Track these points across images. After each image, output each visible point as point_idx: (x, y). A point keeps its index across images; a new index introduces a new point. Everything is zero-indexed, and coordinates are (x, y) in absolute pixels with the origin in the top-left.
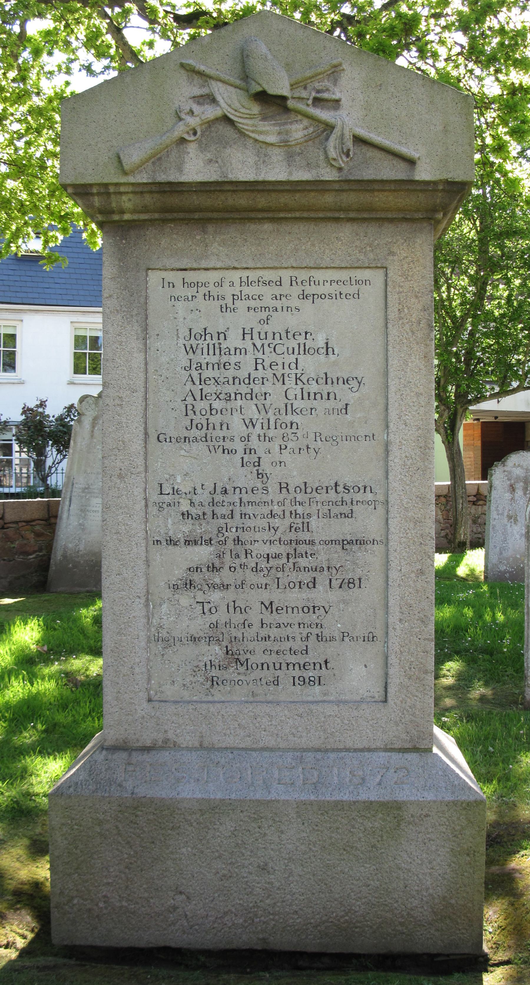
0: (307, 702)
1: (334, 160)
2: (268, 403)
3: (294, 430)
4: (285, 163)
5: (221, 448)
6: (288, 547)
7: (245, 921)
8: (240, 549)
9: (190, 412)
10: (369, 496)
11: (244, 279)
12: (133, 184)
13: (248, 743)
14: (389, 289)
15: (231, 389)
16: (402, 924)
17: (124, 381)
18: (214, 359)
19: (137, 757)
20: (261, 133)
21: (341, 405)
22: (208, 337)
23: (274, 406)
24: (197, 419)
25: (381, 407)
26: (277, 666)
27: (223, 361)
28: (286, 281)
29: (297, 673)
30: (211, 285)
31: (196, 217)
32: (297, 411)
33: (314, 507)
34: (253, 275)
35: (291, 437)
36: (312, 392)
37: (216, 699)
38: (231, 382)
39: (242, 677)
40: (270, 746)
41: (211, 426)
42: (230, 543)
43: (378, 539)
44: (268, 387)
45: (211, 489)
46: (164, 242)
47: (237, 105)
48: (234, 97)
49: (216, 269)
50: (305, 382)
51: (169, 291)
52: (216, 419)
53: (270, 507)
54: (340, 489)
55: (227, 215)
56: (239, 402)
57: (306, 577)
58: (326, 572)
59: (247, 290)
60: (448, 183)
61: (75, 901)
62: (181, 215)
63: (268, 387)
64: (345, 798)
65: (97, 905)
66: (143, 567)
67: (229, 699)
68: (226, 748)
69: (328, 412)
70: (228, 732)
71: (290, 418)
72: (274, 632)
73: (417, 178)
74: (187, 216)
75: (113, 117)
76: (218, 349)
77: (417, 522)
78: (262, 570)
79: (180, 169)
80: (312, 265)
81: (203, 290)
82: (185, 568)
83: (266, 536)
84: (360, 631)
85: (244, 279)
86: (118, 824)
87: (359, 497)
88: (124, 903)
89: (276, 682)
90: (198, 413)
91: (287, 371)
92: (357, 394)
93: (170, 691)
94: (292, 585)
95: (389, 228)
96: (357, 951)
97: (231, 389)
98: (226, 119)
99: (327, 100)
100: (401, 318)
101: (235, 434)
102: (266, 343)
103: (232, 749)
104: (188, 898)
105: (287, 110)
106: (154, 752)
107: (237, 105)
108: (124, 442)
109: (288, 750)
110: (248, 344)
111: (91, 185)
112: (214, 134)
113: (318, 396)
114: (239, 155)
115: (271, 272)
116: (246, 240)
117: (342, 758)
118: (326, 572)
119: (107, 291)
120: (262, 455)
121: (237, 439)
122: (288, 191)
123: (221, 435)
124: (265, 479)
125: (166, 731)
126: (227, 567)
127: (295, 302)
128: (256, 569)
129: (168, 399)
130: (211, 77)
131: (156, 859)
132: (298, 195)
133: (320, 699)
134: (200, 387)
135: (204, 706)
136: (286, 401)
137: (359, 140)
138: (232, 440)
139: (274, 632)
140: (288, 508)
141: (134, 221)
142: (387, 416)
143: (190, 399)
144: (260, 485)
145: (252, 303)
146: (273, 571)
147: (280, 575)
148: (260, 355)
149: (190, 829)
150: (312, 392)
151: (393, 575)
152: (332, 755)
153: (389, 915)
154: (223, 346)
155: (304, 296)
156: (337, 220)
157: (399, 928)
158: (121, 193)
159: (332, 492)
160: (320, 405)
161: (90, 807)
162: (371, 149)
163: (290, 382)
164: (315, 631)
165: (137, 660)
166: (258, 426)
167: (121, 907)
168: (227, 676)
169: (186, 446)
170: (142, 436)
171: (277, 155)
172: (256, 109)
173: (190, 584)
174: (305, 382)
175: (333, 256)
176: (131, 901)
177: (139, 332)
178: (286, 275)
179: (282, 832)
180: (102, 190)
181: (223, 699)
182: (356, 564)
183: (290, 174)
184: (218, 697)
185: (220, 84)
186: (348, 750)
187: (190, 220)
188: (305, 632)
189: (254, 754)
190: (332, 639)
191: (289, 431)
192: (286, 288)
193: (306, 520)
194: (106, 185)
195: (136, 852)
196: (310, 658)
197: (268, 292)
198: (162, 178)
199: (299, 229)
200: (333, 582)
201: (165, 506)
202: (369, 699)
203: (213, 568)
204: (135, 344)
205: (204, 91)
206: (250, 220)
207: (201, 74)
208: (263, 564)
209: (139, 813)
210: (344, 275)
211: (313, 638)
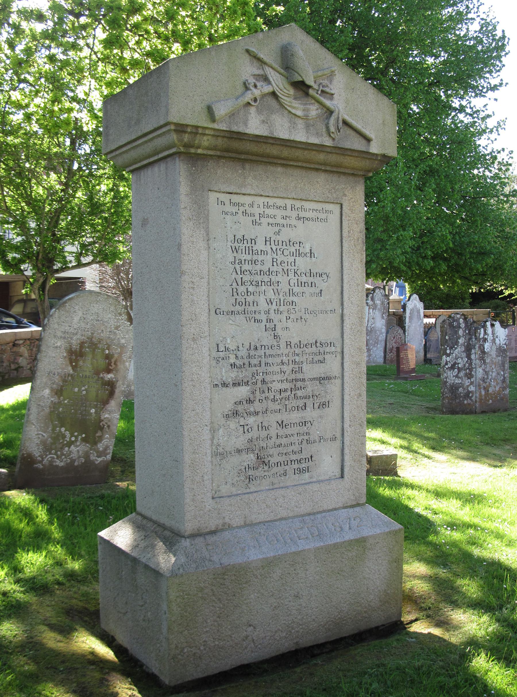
0: (303, 484)
1: (333, 133)
2: (279, 288)
3: (294, 307)
4: (305, 130)
5: (253, 318)
6: (291, 384)
7: (287, 634)
8: (265, 387)
9: (235, 294)
10: (333, 349)
11: (266, 204)
12: (214, 130)
13: (272, 517)
14: (343, 218)
15: (258, 278)
16: (365, 612)
17: (195, 271)
18: (249, 257)
19: (211, 539)
20: (294, 108)
21: (318, 291)
22: (245, 242)
23: (283, 291)
24: (240, 299)
25: (339, 292)
26: (286, 463)
27: (254, 259)
28: (289, 207)
29: (296, 466)
30: (247, 206)
31: (243, 157)
32: (296, 294)
33: (305, 357)
34: (271, 201)
35: (292, 311)
36: (303, 281)
37: (252, 491)
38: (259, 273)
39: (266, 474)
40: (284, 516)
41: (247, 303)
42: (259, 383)
43: (337, 376)
44: (279, 278)
45: (248, 347)
46: (220, 172)
47: (281, 87)
48: (280, 80)
49: (249, 195)
50: (299, 274)
51: (221, 208)
52: (250, 299)
53: (281, 358)
54: (318, 344)
55: (260, 159)
56: (264, 288)
57: (301, 403)
58: (311, 399)
59: (268, 211)
60: (384, 156)
61: (186, 650)
62: (233, 155)
63: (279, 278)
64: (338, 541)
65: (199, 649)
66: (209, 403)
67: (259, 489)
68: (260, 523)
69: (311, 295)
70: (260, 511)
71: (291, 298)
72: (284, 441)
73: (371, 151)
74: (238, 156)
75: (204, 78)
76: (250, 251)
77: (358, 364)
78: (277, 401)
79: (246, 124)
80: (304, 198)
81: (242, 209)
82: (233, 403)
83: (279, 377)
84: (329, 435)
85: (266, 204)
86: (213, 587)
87: (328, 349)
88: (217, 643)
89: (285, 474)
90: (239, 294)
91: (290, 267)
92: (326, 284)
93: (225, 490)
94: (293, 408)
95: (343, 178)
96: (344, 635)
97: (258, 278)
98: (274, 94)
99: (327, 93)
100: (349, 237)
101: (261, 309)
102: (278, 247)
103: (264, 523)
104: (254, 628)
105: (307, 94)
106: (218, 534)
107: (281, 87)
108: (195, 315)
109: (294, 517)
110: (268, 247)
111: (187, 126)
112: (265, 103)
113: (306, 284)
114: (280, 120)
115: (281, 200)
116: (268, 177)
117: (325, 517)
118: (311, 399)
119: (183, 203)
120: (277, 324)
121: (262, 313)
122: (303, 149)
123: (253, 310)
124: (278, 339)
125: (224, 518)
126: (257, 400)
127: (294, 222)
128: (274, 400)
129: (221, 284)
130: (265, 63)
131: (235, 606)
132: (306, 152)
133: (308, 481)
134: (241, 276)
135: (247, 496)
136: (289, 287)
137: (345, 123)
138: (260, 313)
139: (284, 441)
140: (291, 358)
141: (204, 154)
142: (342, 298)
143: (235, 284)
144: (275, 344)
145: (271, 221)
146: (283, 400)
147: (287, 402)
148: (275, 256)
149: (256, 580)
150: (303, 281)
151: (346, 397)
152: (319, 516)
153: (359, 608)
154: (254, 249)
155: (298, 218)
156: (317, 170)
157: (364, 615)
158: (204, 134)
159: (314, 346)
160: (308, 290)
161: (195, 580)
162: (349, 129)
163: (291, 274)
164: (306, 437)
165: (206, 470)
166: (274, 304)
167: (215, 645)
168: (258, 474)
169: (232, 317)
170: (207, 311)
171: (301, 125)
172: (292, 91)
173: (236, 413)
174: (299, 274)
175: (315, 194)
176: (221, 640)
177: (205, 235)
178: (289, 203)
179: (307, 570)
180: (194, 131)
181: (256, 490)
182: (327, 392)
183: (308, 138)
184: (253, 489)
185: (271, 70)
186: (324, 511)
187: (239, 159)
188: (300, 439)
189: (277, 523)
190: (315, 442)
191: (291, 307)
192: (288, 213)
193: (301, 366)
194: (197, 127)
195: (224, 605)
196: (303, 456)
197: (279, 213)
198: (235, 128)
199: (297, 172)
200: (315, 404)
201: (220, 360)
202: (333, 478)
203: (250, 401)
204: (202, 244)
205: (260, 72)
206: (270, 163)
207: (259, 60)
208: (278, 397)
209: (226, 577)
210: (319, 206)
211: (305, 442)
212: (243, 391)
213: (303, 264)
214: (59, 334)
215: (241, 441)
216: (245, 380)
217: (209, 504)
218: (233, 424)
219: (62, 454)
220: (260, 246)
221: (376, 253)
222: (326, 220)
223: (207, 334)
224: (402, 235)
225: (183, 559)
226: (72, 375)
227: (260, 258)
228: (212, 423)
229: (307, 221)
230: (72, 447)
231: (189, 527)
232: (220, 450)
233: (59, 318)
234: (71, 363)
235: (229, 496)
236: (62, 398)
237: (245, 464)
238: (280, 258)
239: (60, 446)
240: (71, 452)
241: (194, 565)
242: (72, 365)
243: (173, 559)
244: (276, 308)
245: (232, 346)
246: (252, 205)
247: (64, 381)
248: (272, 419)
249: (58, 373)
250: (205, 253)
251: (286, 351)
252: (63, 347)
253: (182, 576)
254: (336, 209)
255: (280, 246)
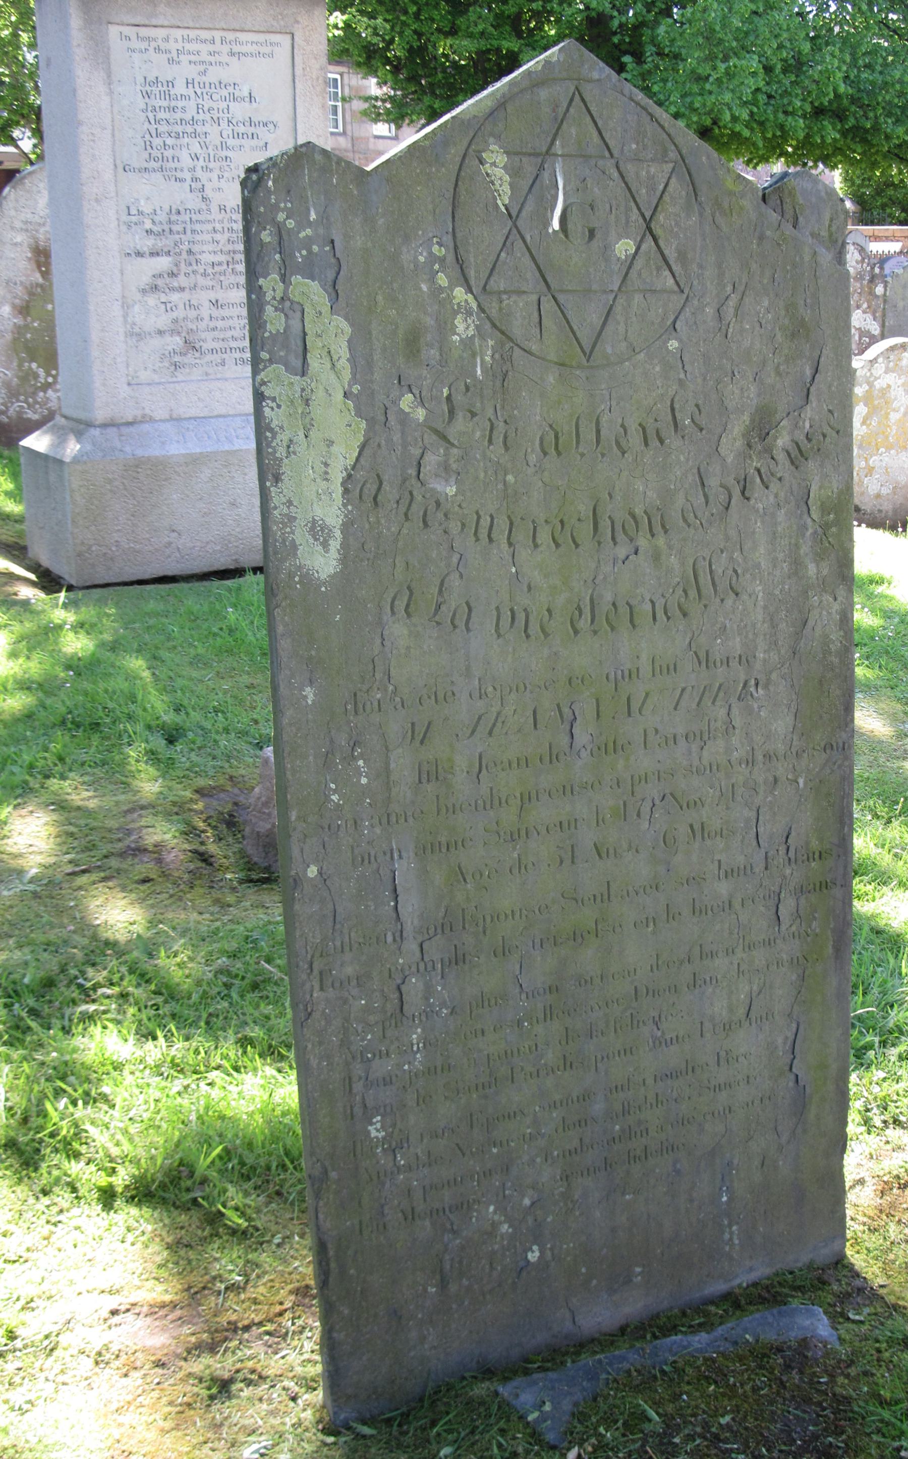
2: (207, 141)
8: (192, 259)
9: (148, 147)
15: (179, 129)
18: (165, 104)
19: (125, 430)
21: (262, 143)
24: (155, 153)
28: (218, 40)
34: (193, 34)
35: (227, 168)
39: (198, 361)
44: (207, 128)
49: (162, 26)
52: (169, 153)
56: (186, 140)
59: (189, 47)
63: (207, 128)
69: (253, 149)
71: (224, 153)
72: (220, 324)
76: (167, 95)
81: (153, 44)
83: (210, 247)
89: (223, 363)
91: (221, 115)
93: (144, 376)
97: (179, 129)
102: (205, 91)
109: (236, 415)
110: (190, 91)
121: (186, 170)
127: (225, 58)
128: (205, 274)
138: (182, 170)
139: (220, 324)
140: (227, 225)
143: (148, 137)
145: (193, 58)
147: (222, 278)
148: (200, 101)
155: (232, 54)
160: (246, 142)
163: (224, 124)
166: (201, 159)
168: (186, 361)
169: (146, 175)
170: (112, 167)
173: (155, 288)
178: (218, 35)
184: (181, 378)
191: (224, 163)
192: (218, 46)
197: (204, 48)
203: (172, 275)
208: (210, 270)
210: (261, 38)
212: (163, 263)
213: (239, 111)
214: (18, 224)
215: (163, 321)
216: (166, 250)
217: (125, 391)
218: (152, 300)
219: (37, 402)
220: (180, 88)
221: (688, 100)
222: (271, 55)
223: (113, 194)
224: (735, 67)
225: (89, 447)
226: (41, 286)
227: (180, 104)
228: (123, 297)
229: (242, 58)
230: (50, 393)
231: (100, 415)
232: (137, 330)
233: (17, 201)
234: (39, 266)
235: (149, 384)
236: (29, 319)
237: (170, 348)
238: (208, 103)
239: (31, 390)
240: (48, 399)
241: (100, 454)
242: (41, 271)
243: (78, 447)
244: (204, 164)
245: (147, 209)
246: (167, 40)
247: (31, 294)
248: (203, 297)
249: (21, 283)
250: (106, 99)
251: (220, 217)
252: (26, 244)
253: (85, 463)
254: (286, 40)
255: (207, 89)
